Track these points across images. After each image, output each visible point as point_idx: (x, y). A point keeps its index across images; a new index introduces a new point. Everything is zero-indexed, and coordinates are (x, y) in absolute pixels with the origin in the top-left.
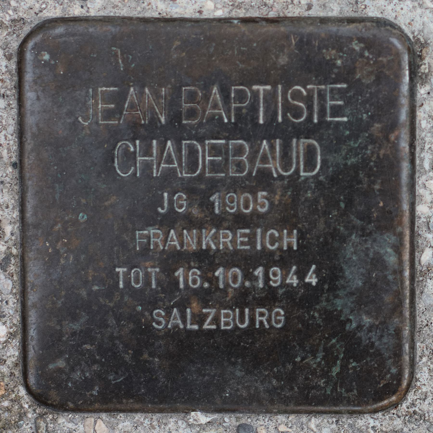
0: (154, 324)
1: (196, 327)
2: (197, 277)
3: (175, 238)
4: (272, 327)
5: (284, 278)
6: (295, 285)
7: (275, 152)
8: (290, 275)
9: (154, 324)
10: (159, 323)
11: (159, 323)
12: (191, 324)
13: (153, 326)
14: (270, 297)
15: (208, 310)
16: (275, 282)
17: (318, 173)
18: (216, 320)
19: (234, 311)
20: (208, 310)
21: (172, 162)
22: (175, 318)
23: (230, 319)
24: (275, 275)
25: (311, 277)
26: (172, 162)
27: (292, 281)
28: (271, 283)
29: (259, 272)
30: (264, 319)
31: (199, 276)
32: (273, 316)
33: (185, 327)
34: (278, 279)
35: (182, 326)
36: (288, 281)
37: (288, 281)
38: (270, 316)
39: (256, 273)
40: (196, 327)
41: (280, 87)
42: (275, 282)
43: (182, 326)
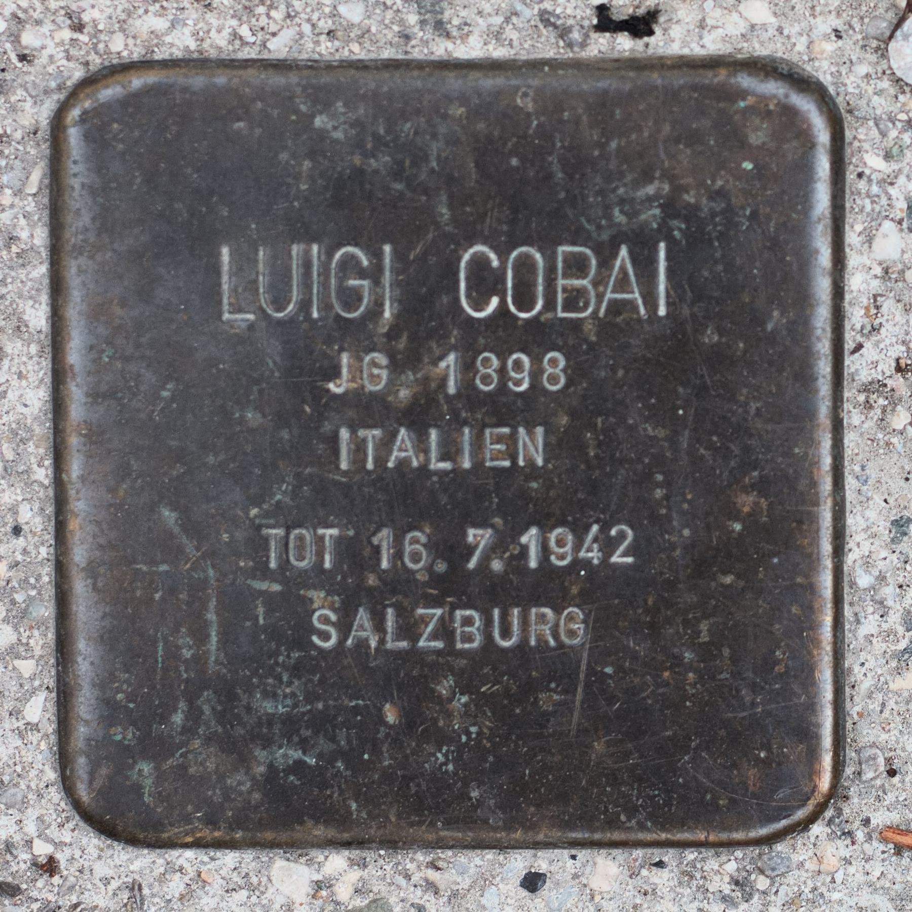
0: (315, 639)
1: (404, 644)
2: (557, 550)
3: (409, 444)
4: (561, 645)
6: (596, 561)
7: (654, 275)
9: (315, 639)
10: (326, 636)
11: (326, 636)
13: (312, 642)
14: (549, 586)
18: (445, 631)
25: (589, 550)
27: (590, 555)
28: (553, 558)
30: (547, 630)
31: (424, 545)
32: (562, 622)
34: (566, 553)
37: (582, 554)
38: (557, 625)
40: (404, 644)
41: (276, 588)
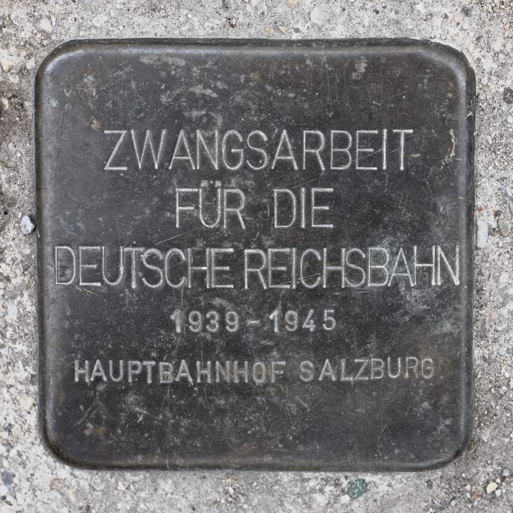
2: (289, 323)
5: (300, 323)
8: (307, 320)
12: (345, 376)
15: (360, 361)
16: (232, 327)
17: (292, 190)
19: (385, 359)
20: (360, 361)
21: (185, 154)
22: (98, 371)
23: (381, 369)
24: (195, 318)
26: (185, 154)
29: (274, 315)
33: (339, 378)
35: (190, 380)
36: (305, 326)
37: (305, 326)
39: (173, 317)
42: (232, 327)
43: (334, 379)
